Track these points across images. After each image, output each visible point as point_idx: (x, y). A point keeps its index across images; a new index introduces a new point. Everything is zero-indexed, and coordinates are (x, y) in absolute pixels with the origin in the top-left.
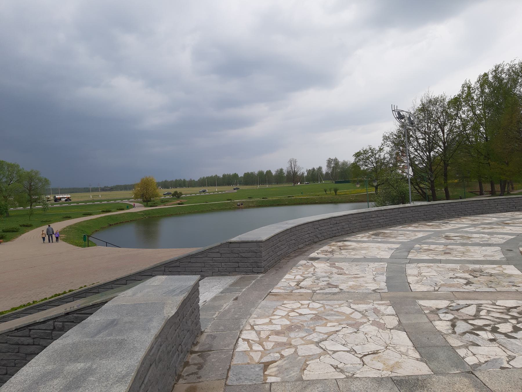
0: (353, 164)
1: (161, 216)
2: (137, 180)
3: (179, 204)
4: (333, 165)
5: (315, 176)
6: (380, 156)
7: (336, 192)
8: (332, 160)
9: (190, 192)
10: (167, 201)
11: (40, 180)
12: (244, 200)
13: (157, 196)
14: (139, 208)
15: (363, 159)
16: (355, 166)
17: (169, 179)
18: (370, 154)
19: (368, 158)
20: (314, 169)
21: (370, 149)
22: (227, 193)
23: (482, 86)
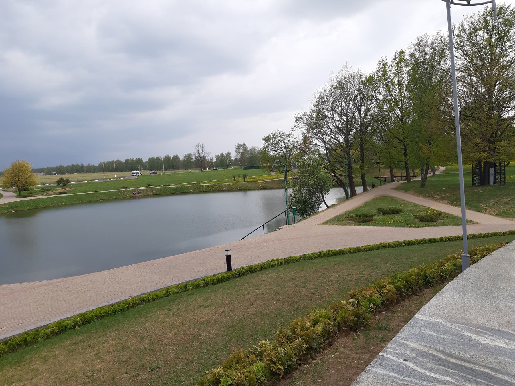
3: (61, 193)
4: (241, 151)
5: (223, 162)
10: (48, 190)
12: (140, 188)
15: (272, 144)
16: (264, 152)
17: (65, 164)
18: (279, 138)
19: (277, 143)
20: (222, 154)
22: (125, 180)
23: (398, 65)
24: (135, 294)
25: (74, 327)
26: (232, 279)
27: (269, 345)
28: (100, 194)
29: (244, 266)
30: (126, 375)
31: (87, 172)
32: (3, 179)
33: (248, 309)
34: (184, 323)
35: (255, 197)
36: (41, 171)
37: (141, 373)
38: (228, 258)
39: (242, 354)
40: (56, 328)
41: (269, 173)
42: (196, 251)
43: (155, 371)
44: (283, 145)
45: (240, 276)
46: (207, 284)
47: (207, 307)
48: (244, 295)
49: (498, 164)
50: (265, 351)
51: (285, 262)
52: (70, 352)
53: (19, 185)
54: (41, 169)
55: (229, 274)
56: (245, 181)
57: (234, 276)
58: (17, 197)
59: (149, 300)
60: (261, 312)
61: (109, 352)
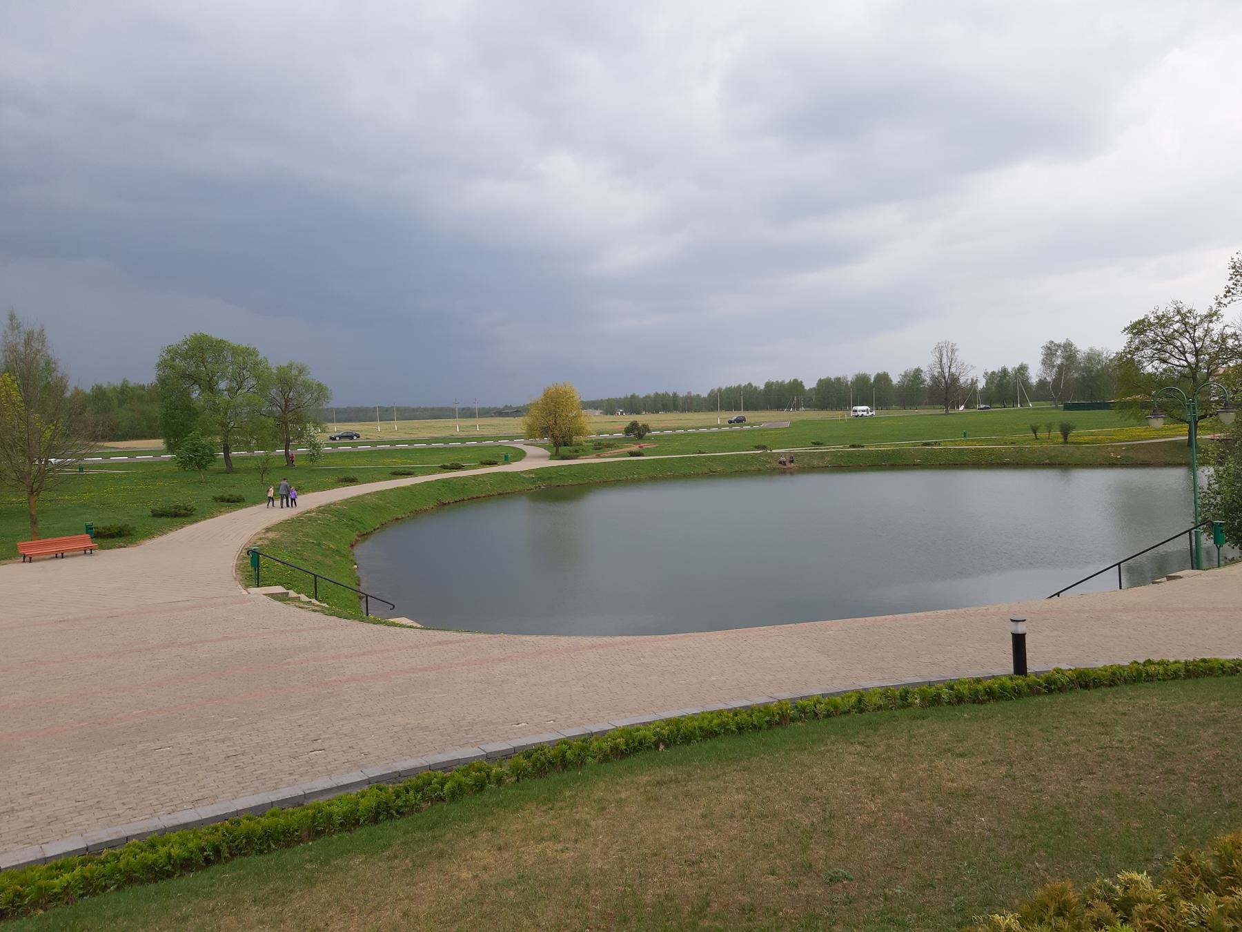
0: (1120, 357)
1: (417, 513)
2: (530, 393)
3: (632, 454)
4: (1059, 362)
5: (1007, 389)
6: (1207, 332)
7: (1065, 436)
8: (1059, 346)
9: (675, 424)
10: (608, 446)
11: (308, 387)
13: (579, 432)
14: (536, 459)
15: (1154, 342)
16: (1126, 365)
17: (644, 390)
18: (1176, 326)
19: (1169, 339)
20: (1004, 371)
21: (1179, 312)
22: (763, 429)
24: (785, 695)
25: (657, 745)
26: (1027, 695)
27: (1149, 886)
28: (708, 458)
29: (1064, 667)
30: (771, 878)
31: (683, 411)
32: (527, 419)
33: (1079, 780)
34: (905, 785)
35: (1094, 488)
36: (595, 405)
37: (808, 882)
38: (1019, 642)
39: (1071, 895)
40: (621, 741)
41: (1143, 421)
42: (929, 613)
43: (840, 885)
44: (1188, 345)
45: (1050, 691)
46: (959, 699)
47: (962, 755)
48: (1065, 744)
50: (1140, 901)
51: (1187, 671)
52: (649, 799)
53: (557, 433)
54: (597, 402)
55: (1020, 681)
56: (1066, 442)
57: (1034, 690)
58: (552, 458)
59: (816, 714)
60: (1117, 795)
61: (732, 817)
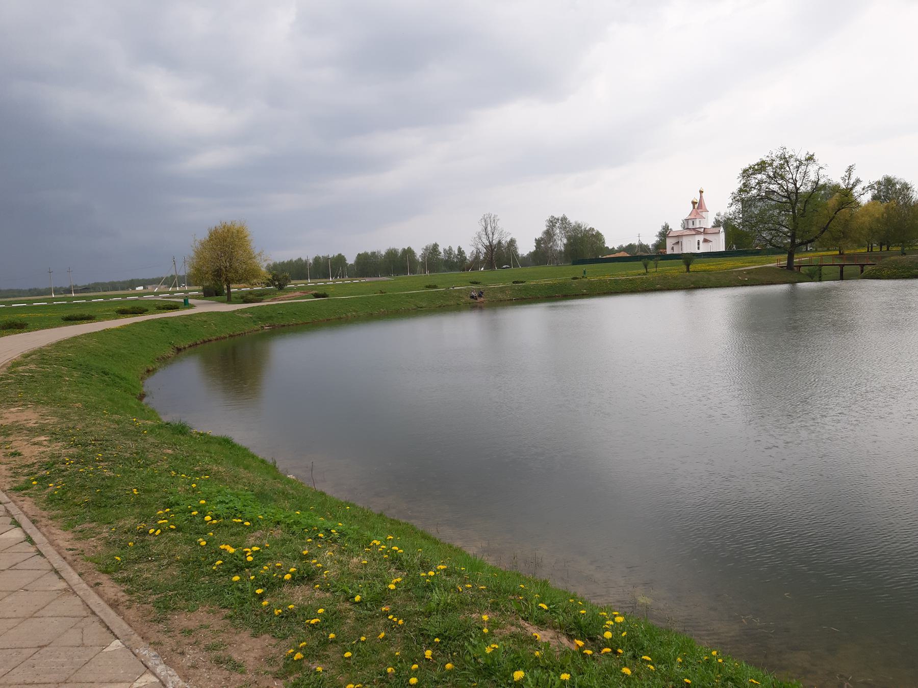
28: (407, 295)
49: (158, 670)
